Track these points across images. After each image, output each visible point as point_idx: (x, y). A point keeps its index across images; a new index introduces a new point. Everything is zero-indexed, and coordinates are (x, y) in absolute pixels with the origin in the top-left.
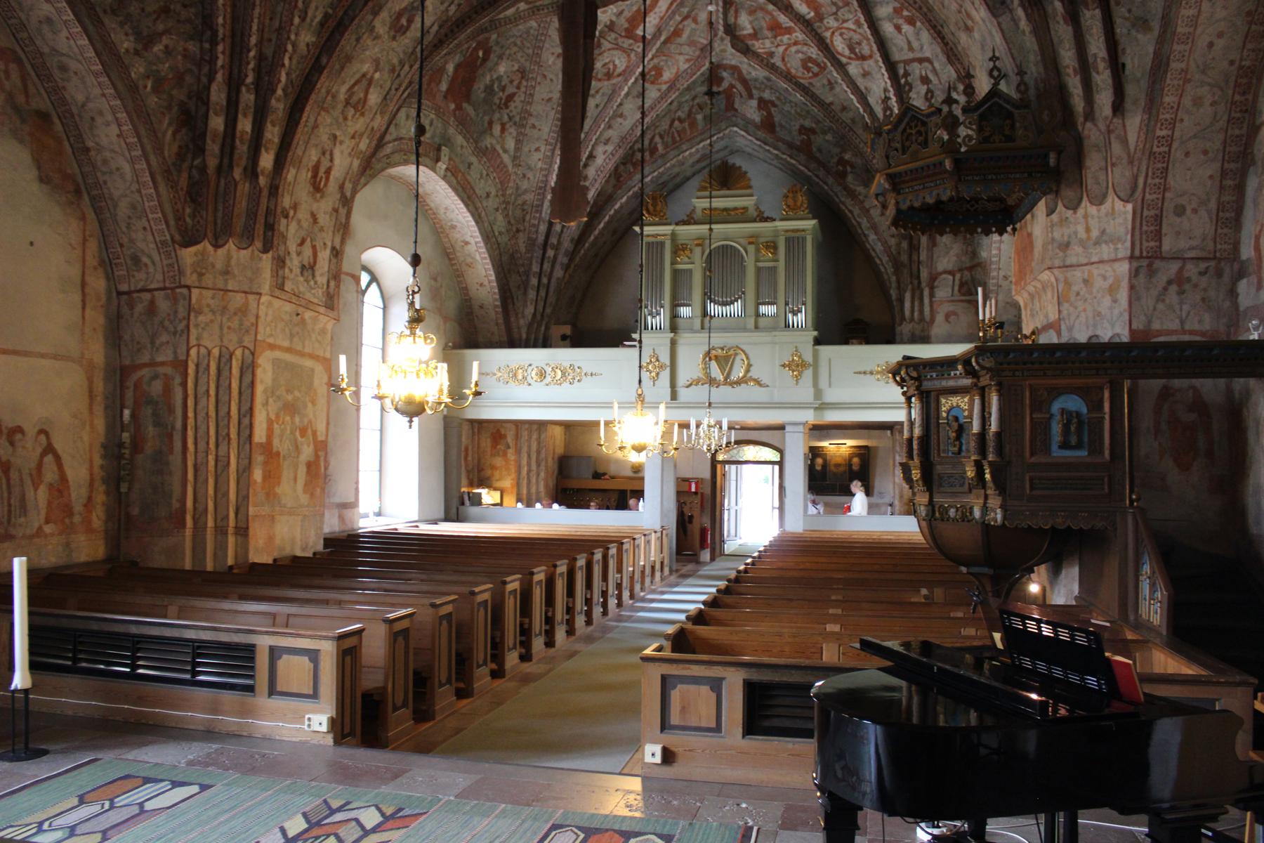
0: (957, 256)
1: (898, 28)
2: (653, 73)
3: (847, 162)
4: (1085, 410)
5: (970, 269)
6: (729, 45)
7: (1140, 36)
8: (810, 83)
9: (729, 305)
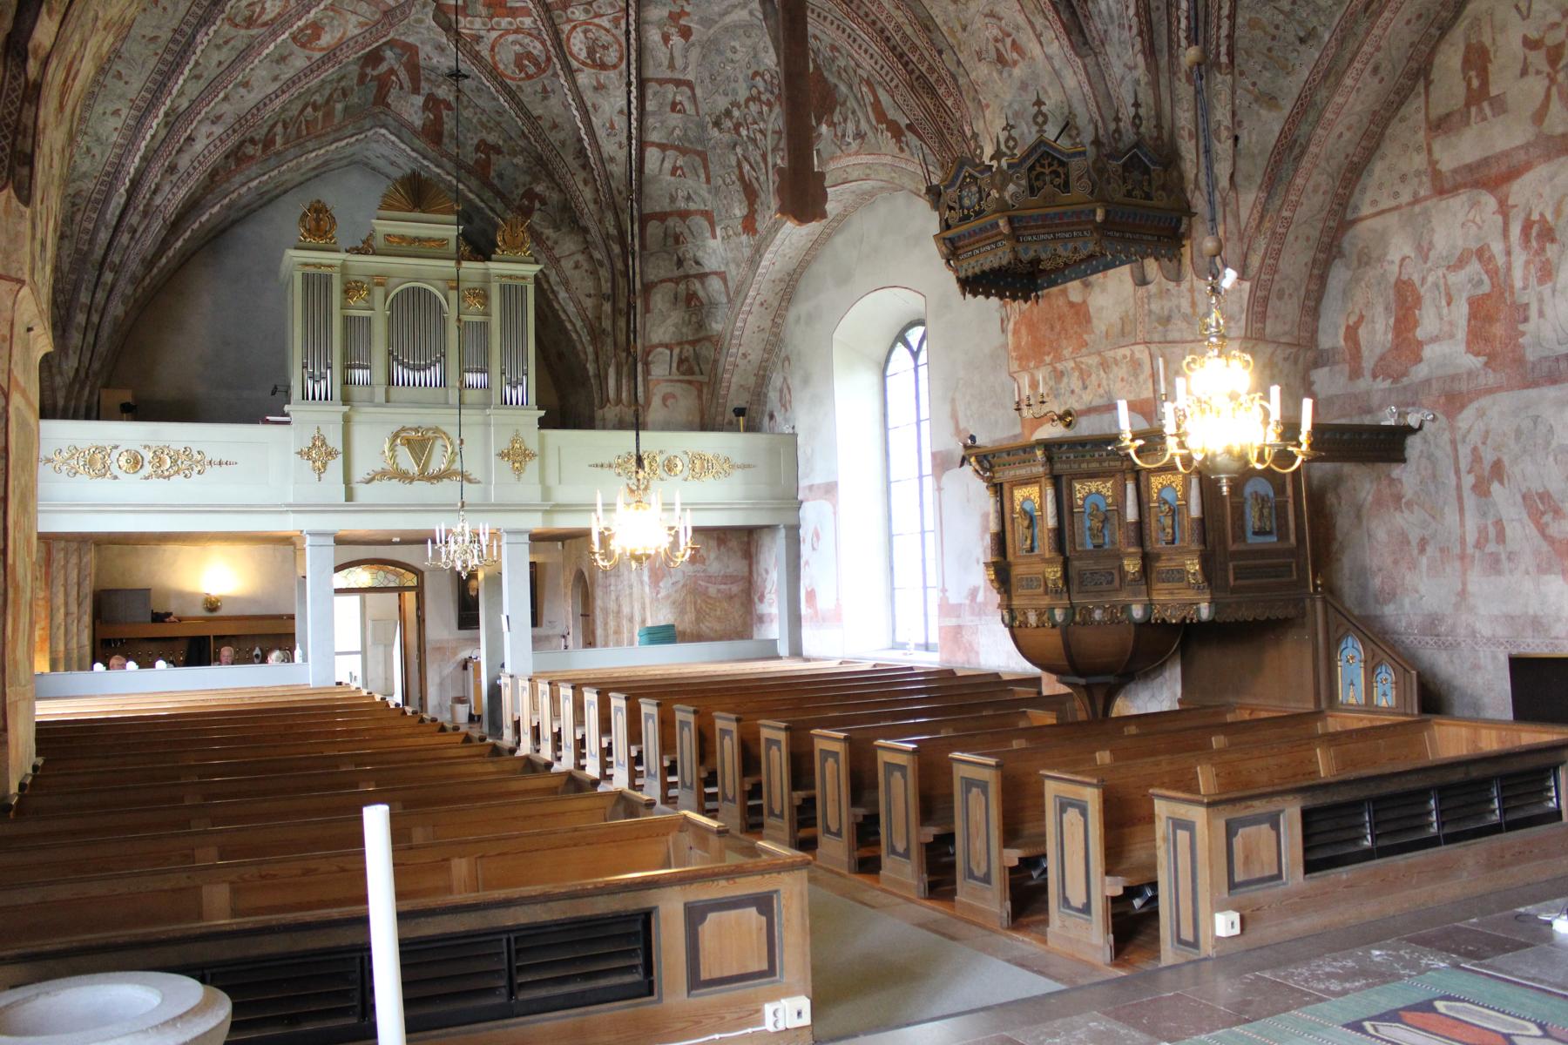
0: (676, 325)
1: (666, 38)
2: (309, 32)
3: (537, 196)
4: (1271, 494)
5: (693, 343)
6: (431, 15)
7: (1263, 112)
8: (519, 87)
9: (425, 370)
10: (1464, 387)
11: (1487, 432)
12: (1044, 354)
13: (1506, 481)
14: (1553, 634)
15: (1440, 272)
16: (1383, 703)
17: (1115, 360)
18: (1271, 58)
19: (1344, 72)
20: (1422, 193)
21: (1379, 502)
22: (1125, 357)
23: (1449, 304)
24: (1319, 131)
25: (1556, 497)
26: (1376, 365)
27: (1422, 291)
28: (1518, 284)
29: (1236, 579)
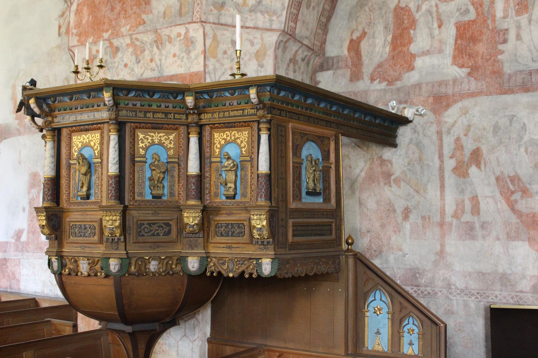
10: (450, 91)
11: (469, 126)
13: (482, 166)
14: (519, 288)
17: (169, 37)
21: (371, 178)
22: (179, 35)
23: (440, 27)
25: (524, 179)
26: (374, 71)
27: (417, 16)
28: (499, 13)
29: (294, 235)
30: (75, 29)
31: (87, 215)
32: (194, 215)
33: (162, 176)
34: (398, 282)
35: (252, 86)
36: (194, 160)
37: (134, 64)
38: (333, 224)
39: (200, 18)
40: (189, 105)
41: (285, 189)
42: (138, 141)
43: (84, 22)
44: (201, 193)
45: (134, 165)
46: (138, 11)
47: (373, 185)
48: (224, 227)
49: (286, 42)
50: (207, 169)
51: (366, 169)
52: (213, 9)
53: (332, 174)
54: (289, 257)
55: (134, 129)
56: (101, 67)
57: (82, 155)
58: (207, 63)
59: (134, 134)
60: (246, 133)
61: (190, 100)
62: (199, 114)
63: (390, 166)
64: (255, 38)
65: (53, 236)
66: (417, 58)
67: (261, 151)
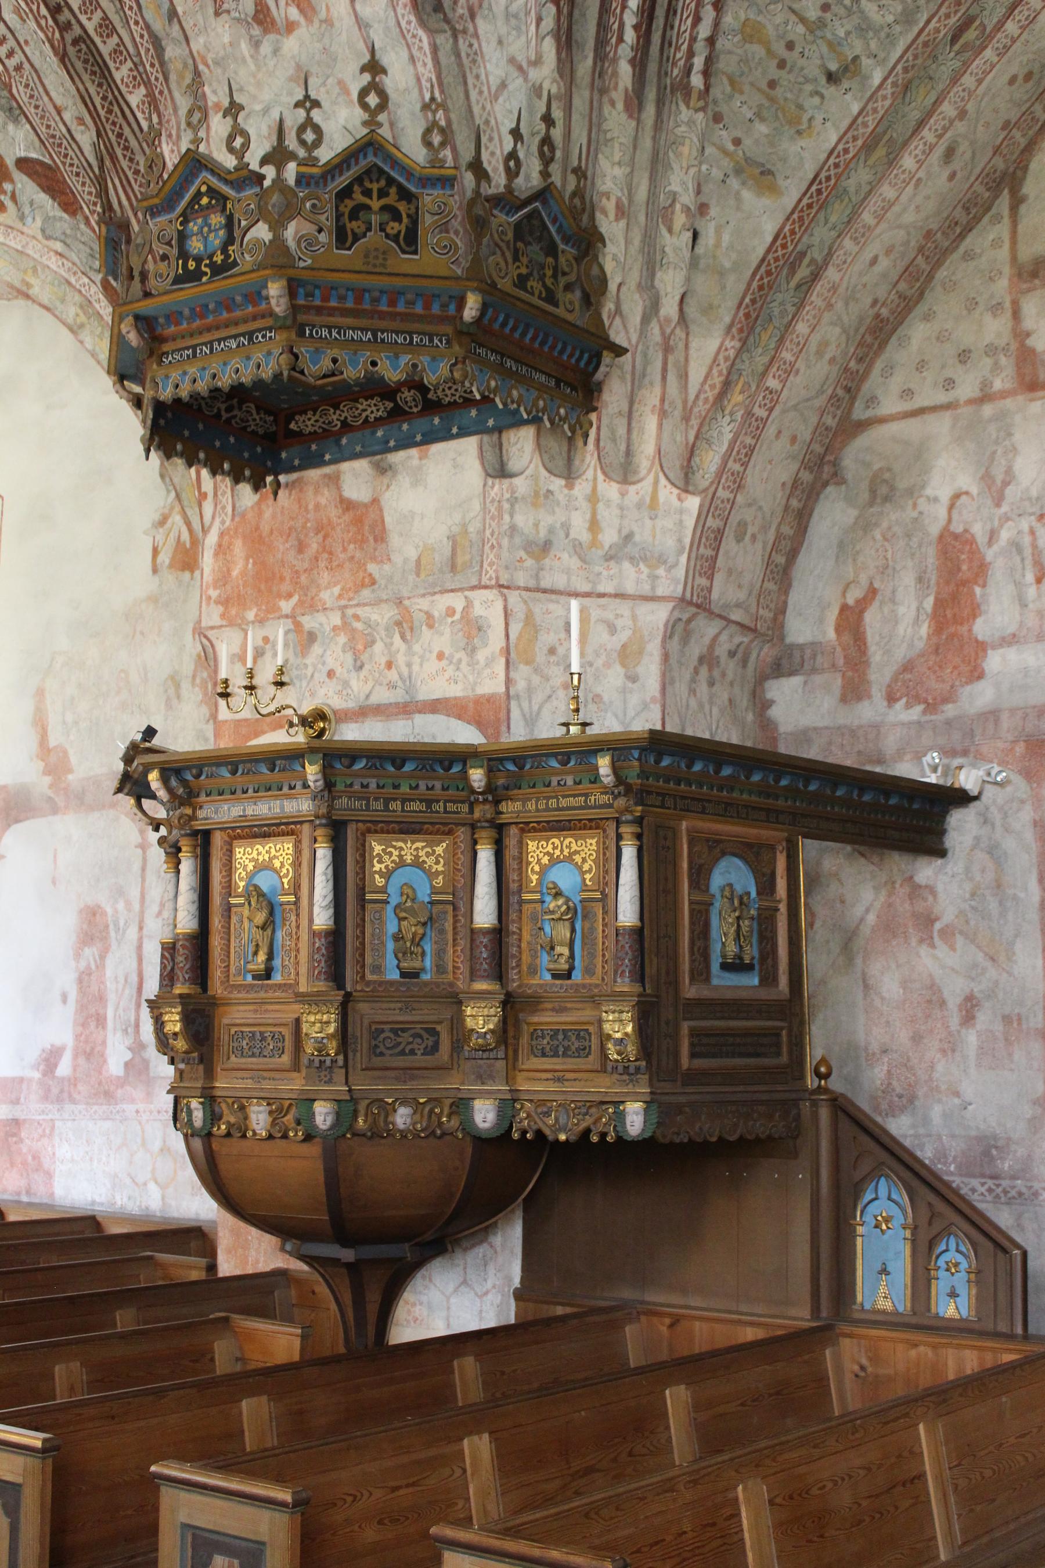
7: (747, 195)
12: (279, 596)
15: (1025, 525)
16: (949, 1310)
17: (429, 615)
18: (772, 100)
19: (906, 143)
20: (998, 385)
21: (889, 927)
22: (451, 612)
24: (848, 243)
26: (895, 679)
27: (990, 554)
29: (693, 1055)
30: (215, 588)
31: (266, 1011)
32: (486, 1012)
33: (421, 931)
34: (927, 1162)
35: (602, 750)
36: (487, 897)
37: (349, 671)
38: (784, 1032)
39: (497, 578)
40: (476, 785)
41: (674, 958)
42: (372, 858)
43: (235, 573)
44: (500, 966)
45: (363, 908)
46: (358, 554)
47: (894, 943)
48: (548, 1038)
49: (689, 621)
50: (513, 916)
51: (878, 905)
52: (524, 556)
53: (780, 924)
54: (682, 1099)
55: (363, 835)
56: (280, 684)
57: (256, 887)
58: (512, 674)
59: (364, 845)
60: (594, 841)
61: (477, 776)
62: (497, 802)
63: (931, 898)
64: (617, 616)
65: (195, 1054)
66: (989, 652)
67: (621, 882)
